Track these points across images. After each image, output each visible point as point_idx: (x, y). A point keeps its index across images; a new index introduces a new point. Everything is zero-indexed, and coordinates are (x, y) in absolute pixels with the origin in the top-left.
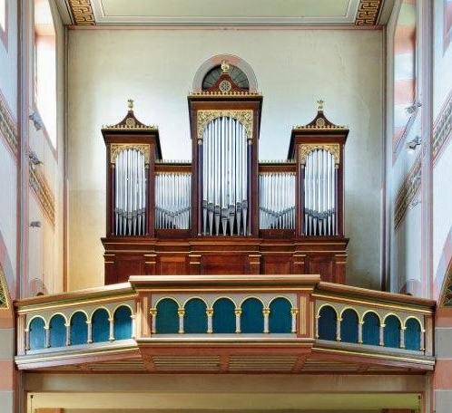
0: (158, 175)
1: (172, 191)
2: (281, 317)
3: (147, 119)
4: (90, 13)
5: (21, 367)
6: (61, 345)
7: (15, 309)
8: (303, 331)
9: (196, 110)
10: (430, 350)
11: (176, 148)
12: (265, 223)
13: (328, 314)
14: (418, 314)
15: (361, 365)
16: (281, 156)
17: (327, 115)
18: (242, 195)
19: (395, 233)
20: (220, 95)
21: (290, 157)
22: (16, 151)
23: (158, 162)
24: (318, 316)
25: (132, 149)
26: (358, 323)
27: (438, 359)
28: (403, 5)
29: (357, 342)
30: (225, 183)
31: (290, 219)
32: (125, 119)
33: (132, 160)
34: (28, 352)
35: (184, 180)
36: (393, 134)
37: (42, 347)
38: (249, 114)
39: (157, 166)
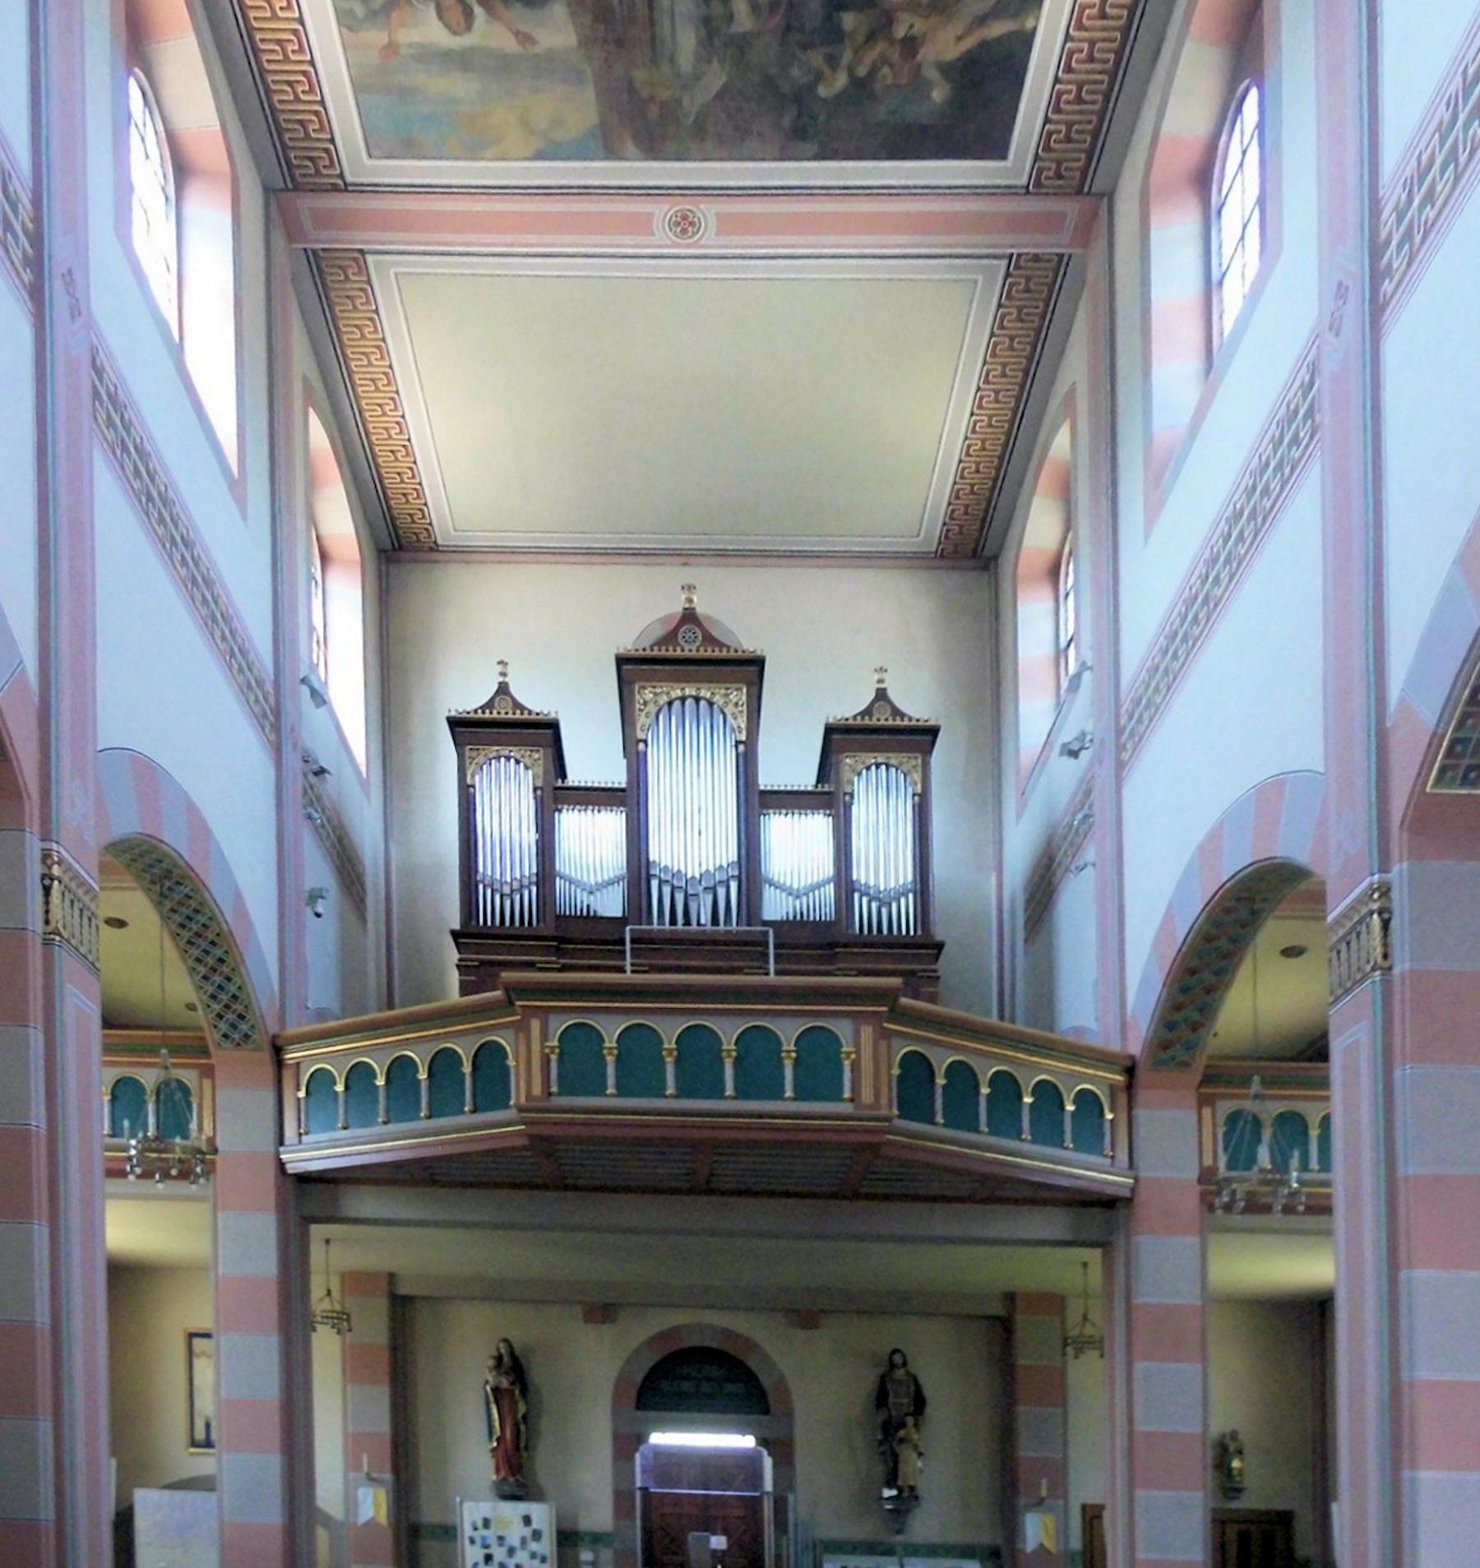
0: (560, 811)
1: (591, 846)
2: (820, 1065)
3: (535, 700)
4: (394, 416)
5: (291, 1169)
6: (369, 1122)
7: (278, 1051)
8: (867, 1096)
9: (631, 683)
10: (1123, 1156)
11: (593, 758)
12: (775, 906)
13: (916, 1070)
14: (1100, 1081)
15: (984, 1178)
16: (805, 777)
17: (892, 695)
18: (727, 852)
19: (1026, 953)
20: (679, 652)
21: (822, 777)
22: (27, 277)
23: (559, 783)
24: (896, 1071)
25: (508, 758)
26: (977, 1093)
27: (1142, 1174)
28: (1189, 48)
29: (977, 1131)
30: (693, 835)
31: (825, 903)
32: (492, 700)
33: (508, 794)
34: (305, 1139)
35: (611, 824)
36: (1018, 766)
37: (334, 1129)
38: (739, 695)
39: (557, 793)
